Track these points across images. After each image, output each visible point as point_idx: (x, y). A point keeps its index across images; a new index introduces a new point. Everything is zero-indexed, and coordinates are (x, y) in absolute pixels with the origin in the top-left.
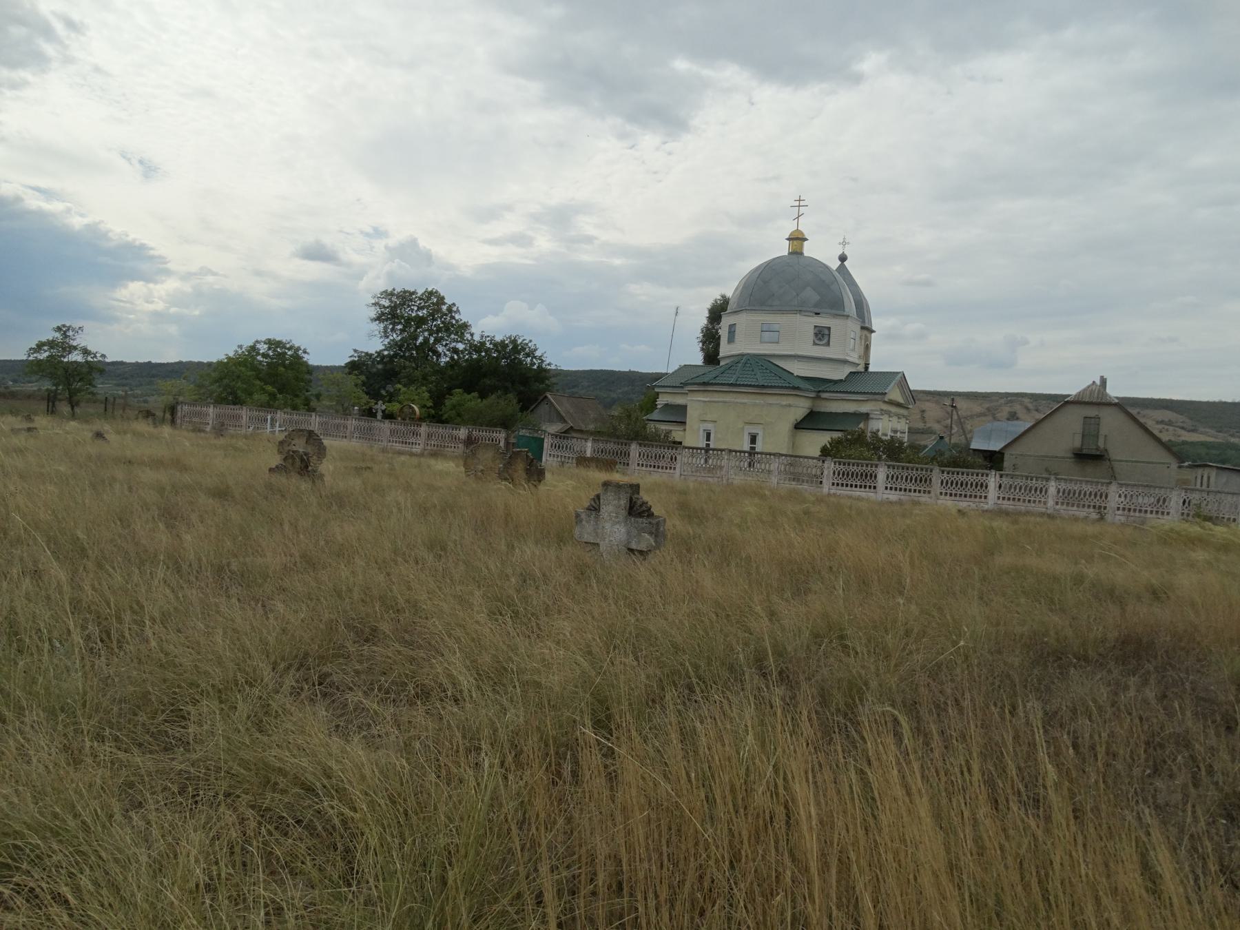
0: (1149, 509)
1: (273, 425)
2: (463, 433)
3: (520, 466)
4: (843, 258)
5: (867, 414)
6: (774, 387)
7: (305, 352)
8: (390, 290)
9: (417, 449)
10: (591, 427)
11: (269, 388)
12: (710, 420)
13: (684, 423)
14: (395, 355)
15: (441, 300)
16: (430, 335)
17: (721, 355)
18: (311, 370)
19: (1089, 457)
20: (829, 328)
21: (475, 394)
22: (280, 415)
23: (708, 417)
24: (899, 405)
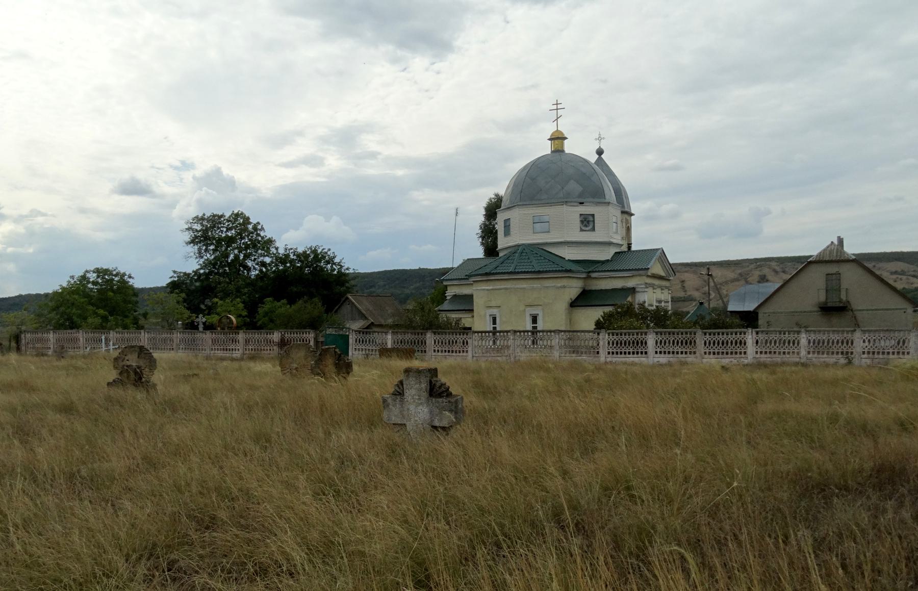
0: (891, 351)
1: (107, 344)
2: (276, 336)
4: (600, 152)
7: (130, 277)
10: (390, 321)
11: (101, 312)
13: (472, 310)
14: (211, 273)
15: (247, 220)
17: (499, 247)
18: (136, 292)
19: (834, 309)
20: (593, 215)
21: (284, 301)
22: (112, 335)
23: (493, 304)
24: (661, 278)
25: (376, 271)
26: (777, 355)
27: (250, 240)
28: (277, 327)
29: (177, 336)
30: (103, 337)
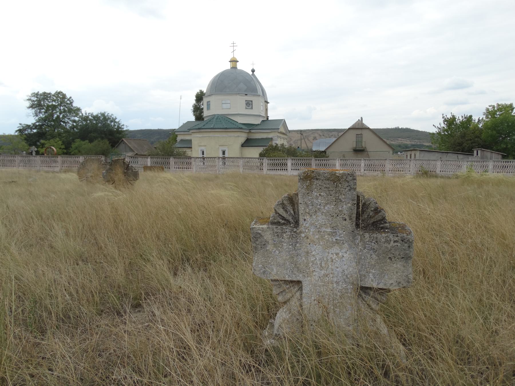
0: (402, 170)
3: (119, 172)
4: (253, 71)
5: (272, 138)
6: (231, 128)
8: (36, 92)
9: (57, 169)
12: (202, 144)
13: (191, 147)
14: (43, 125)
15: (64, 96)
16: (60, 114)
19: (359, 151)
20: (252, 101)
21: (87, 141)
23: (202, 144)
24: (283, 134)
25: (136, 129)
28: (82, 154)
29: (18, 159)
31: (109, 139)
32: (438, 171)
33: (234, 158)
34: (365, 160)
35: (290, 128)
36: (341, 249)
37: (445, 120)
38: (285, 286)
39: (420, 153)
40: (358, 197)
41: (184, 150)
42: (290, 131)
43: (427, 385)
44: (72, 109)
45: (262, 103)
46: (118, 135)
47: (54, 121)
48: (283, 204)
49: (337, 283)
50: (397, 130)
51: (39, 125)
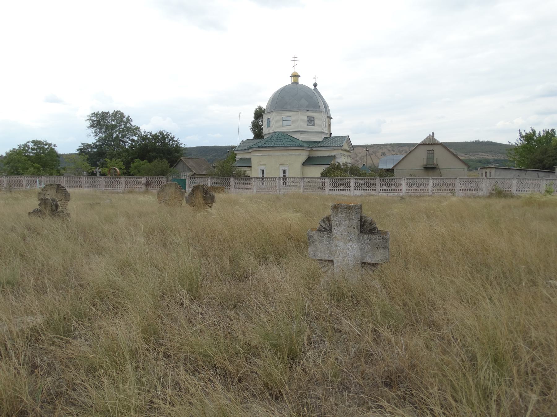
1: (40, 184)
2: (144, 180)
4: (315, 85)
5: (335, 156)
7: (55, 146)
8: (96, 112)
9: (120, 190)
10: (204, 173)
11: (36, 165)
12: (263, 164)
14: (103, 144)
15: (122, 115)
16: (119, 133)
17: (264, 133)
18: (59, 156)
19: (430, 168)
20: (314, 117)
21: (146, 161)
22: (43, 179)
24: (347, 151)
26: (520, 192)
27: (125, 127)
28: (144, 175)
30: (38, 180)
31: (168, 159)
32: (514, 191)
33: (295, 178)
34: (434, 179)
35: (354, 143)
36: (353, 243)
37: (522, 137)
38: (325, 263)
39: (495, 171)
40: (361, 217)
41: (245, 169)
42: (354, 147)
43: (500, 416)
44: (130, 128)
45: (325, 119)
46: (176, 154)
47: (113, 140)
48: (324, 221)
49: (351, 261)
50: (477, 143)
51: (99, 145)
